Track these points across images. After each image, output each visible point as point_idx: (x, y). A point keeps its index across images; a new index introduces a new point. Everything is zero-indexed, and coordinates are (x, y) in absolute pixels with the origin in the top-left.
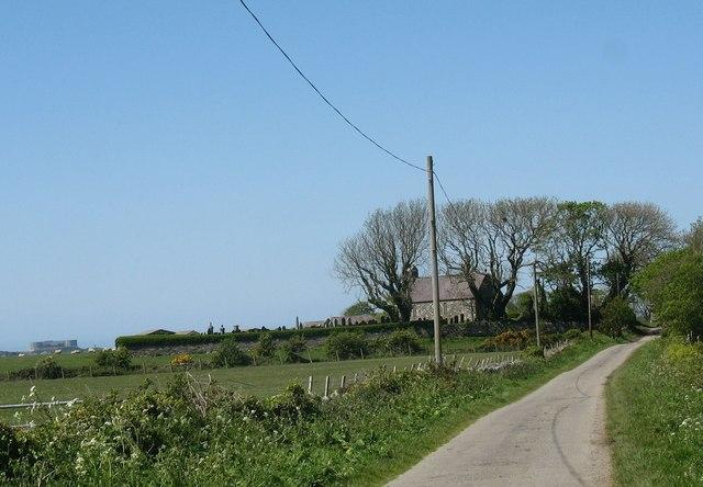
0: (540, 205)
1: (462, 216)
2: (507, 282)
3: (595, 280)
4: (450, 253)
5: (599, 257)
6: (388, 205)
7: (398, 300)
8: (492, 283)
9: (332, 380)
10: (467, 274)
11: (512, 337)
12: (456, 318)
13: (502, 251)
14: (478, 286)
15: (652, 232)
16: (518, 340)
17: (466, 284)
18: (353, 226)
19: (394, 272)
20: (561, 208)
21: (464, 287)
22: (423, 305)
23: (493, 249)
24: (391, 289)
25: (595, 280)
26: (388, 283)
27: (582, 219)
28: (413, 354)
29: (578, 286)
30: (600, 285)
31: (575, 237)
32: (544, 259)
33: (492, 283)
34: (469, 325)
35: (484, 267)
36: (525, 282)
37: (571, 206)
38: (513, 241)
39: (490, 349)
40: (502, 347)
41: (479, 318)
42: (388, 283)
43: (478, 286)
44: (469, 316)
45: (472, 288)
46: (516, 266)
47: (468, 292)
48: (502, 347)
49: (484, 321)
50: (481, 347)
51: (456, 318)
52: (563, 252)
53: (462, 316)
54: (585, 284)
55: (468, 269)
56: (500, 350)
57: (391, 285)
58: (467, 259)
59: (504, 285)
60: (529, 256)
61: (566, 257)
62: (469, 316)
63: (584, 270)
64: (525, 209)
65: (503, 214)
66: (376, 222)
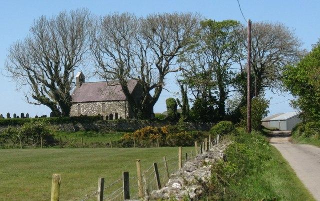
0: (186, 21)
1: (117, 28)
2: (155, 86)
3: (230, 88)
4: (107, 59)
5: (235, 68)
6: (51, 14)
7: (57, 96)
8: (143, 86)
9: (167, 158)
10: (121, 79)
11: (151, 132)
12: (111, 116)
13: (151, 57)
14: (131, 89)
15: (282, 48)
16: (158, 136)
17: (120, 87)
18: (22, 33)
19: (57, 72)
20: (204, 25)
21: (118, 90)
22: (86, 104)
23: (143, 59)
24: (52, 87)
25: (230, 88)
26: (49, 82)
27: (218, 34)
28: (46, 146)
29: (215, 93)
30: (234, 96)
31: (216, 51)
32: (189, 68)
33: (143, 86)
34: (121, 122)
35: (135, 73)
36: (172, 89)
37: (210, 23)
38: (161, 48)
39: (129, 144)
40: (141, 142)
41: (131, 116)
42: (49, 82)
43: (131, 89)
44: (123, 114)
45: (125, 90)
46: (163, 72)
47: (122, 96)
48: (141, 142)
49: (134, 119)
50: (120, 142)
51: (111, 116)
52: (202, 61)
53: (117, 114)
54: (222, 89)
55: (122, 72)
56: (139, 145)
57: (53, 83)
58: (121, 63)
59: (152, 87)
60: (174, 64)
61: (207, 67)
62: (123, 114)
63: (222, 76)
64: (172, 22)
65: (152, 27)
66: (40, 28)
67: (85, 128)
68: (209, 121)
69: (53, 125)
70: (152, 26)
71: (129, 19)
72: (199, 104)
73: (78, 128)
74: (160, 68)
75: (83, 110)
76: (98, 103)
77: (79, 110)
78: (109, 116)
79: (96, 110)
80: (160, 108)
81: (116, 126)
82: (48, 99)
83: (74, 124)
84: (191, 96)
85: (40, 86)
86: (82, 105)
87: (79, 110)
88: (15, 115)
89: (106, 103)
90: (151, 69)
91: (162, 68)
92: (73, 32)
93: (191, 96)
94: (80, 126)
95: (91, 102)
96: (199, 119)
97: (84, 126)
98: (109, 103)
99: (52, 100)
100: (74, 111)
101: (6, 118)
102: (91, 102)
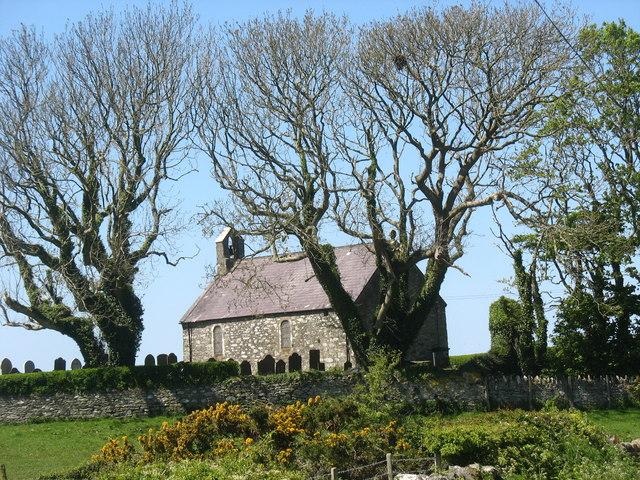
20: (590, 42)
22: (235, 325)
23: (379, 172)
64: (461, 36)
67: (184, 405)
68: (612, 372)
69: (73, 394)
70: (398, 51)
71: (320, 29)
72: (579, 312)
73: (159, 403)
74: (434, 197)
75: (229, 344)
76: (268, 320)
77: (217, 344)
78: (286, 361)
79: (262, 344)
80: (468, 334)
81: (291, 393)
82: (68, 313)
83: (147, 390)
84: (554, 290)
85: (40, 270)
86: (224, 327)
87: (217, 344)
88: (29, 366)
89: (292, 321)
90: (415, 201)
91: (442, 194)
92: (133, 91)
93: (554, 290)
94: (165, 397)
95: (250, 318)
96: (577, 367)
97: (180, 398)
98: (300, 319)
99: (78, 314)
100: (202, 349)
101: (22, 370)
102: (250, 318)
